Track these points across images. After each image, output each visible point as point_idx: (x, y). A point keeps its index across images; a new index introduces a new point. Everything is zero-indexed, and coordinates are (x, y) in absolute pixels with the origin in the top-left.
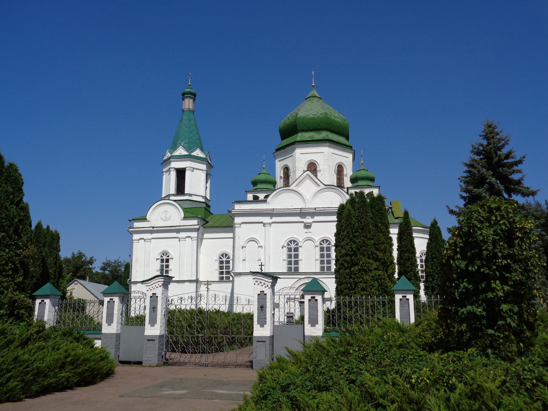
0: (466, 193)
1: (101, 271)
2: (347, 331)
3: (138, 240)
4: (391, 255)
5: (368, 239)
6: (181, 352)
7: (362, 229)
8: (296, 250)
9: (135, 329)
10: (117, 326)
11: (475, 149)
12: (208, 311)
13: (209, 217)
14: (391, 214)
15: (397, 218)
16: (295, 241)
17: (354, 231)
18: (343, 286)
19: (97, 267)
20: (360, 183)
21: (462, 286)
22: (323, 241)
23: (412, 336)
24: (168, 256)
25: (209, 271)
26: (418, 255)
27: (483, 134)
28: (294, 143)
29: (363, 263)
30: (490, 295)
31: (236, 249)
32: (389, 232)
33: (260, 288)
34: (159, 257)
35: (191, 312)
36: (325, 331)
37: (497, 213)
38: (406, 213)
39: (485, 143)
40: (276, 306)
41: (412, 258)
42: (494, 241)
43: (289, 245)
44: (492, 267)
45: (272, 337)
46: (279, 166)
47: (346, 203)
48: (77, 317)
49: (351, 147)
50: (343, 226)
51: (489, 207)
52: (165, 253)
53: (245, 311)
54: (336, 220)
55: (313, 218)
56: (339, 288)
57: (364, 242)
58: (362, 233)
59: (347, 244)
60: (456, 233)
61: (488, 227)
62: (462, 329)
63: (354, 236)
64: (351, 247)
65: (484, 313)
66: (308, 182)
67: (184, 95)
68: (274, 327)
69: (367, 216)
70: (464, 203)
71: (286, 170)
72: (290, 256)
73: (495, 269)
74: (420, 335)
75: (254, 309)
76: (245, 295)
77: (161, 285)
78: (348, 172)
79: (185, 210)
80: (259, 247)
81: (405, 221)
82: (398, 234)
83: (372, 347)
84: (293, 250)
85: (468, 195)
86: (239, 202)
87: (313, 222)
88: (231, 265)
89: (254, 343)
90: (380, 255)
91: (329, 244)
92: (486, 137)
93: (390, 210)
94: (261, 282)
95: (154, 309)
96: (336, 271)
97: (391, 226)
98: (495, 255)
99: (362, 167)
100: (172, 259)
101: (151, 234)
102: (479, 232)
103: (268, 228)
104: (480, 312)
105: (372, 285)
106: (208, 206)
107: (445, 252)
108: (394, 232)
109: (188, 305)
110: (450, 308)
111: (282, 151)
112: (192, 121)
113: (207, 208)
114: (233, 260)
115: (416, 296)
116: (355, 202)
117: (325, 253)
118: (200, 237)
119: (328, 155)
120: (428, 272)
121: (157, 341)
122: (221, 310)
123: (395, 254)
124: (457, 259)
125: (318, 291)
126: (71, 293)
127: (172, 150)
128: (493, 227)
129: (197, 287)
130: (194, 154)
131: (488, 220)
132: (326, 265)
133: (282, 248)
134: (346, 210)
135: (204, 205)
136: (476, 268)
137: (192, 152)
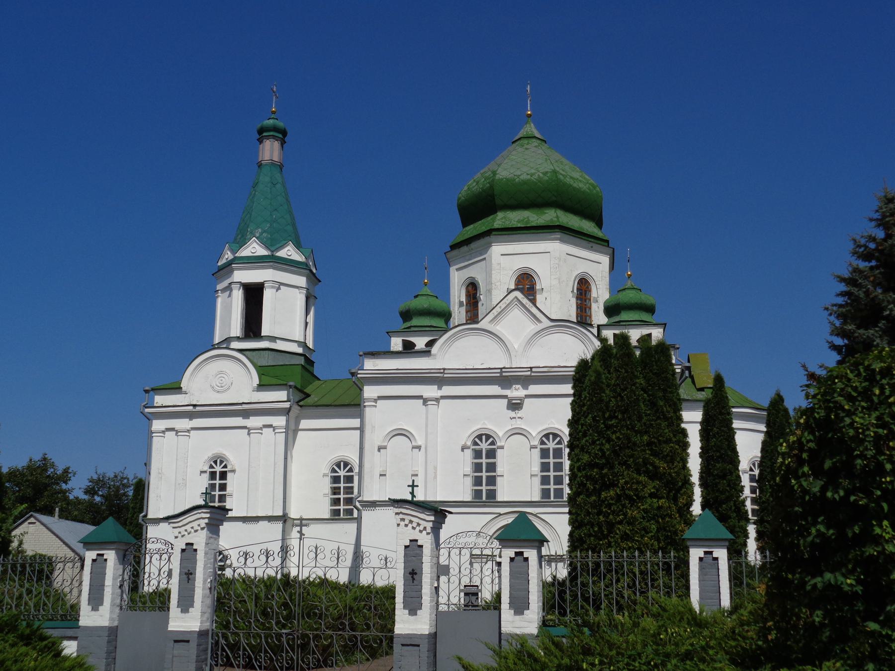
0: (843, 338)
1: (86, 497)
2: (586, 624)
3: (163, 432)
4: (685, 467)
5: (637, 432)
6: (245, 667)
7: (623, 413)
8: (491, 454)
9: (148, 617)
10: (111, 612)
11: (860, 246)
12: (304, 581)
13: (310, 385)
14: (689, 380)
15: (702, 389)
16: (488, 437)
17: (607, 415)
18: (584, 531)
19: (77, 488)
20: (625, 316)
21: (813, 531)
22: (547, 436)
23: (717, 635)
24: (225, 466)
25: (310, 497)
26: (744, 465)
27: (877, 216)
28: (488, 233)
29: (626, 483)
30: (871, 551)
31: (418, 450)
32: (680, 419)
33: (409, 534)
34: (206, 468)
35: (269, 583)
36: (544, 624)
37: (884, 381)
38: (719, 380)
39: (880, 234)
40: (442, 570)
41: (731, 473)
42: (877, 437)
43: (475, 444)
44: (873, 493)
45: (433, 637)
46: (457, 279)
47: (593, 358)
48: (29, 592)
49: (607, 241)
50: (584, 405)
51: (867, 368)
52: (218, 460)
53: (380, 583)
54: (572, 392)
55: (525, 387)
56: (576, 534)
57: (629, 439)
58: (624, 420)
59: (594, 442)
60: (802, 421)
61: (868, 409)
62: (814, 621)
63: (608, 427)
64: (601, 450)
65: (859, 589)
66: (516, 314)
67: (262, 133)
68: (440, 617)
69: (634, 384)
70: (839, 358)
71: (472, 288)
72: (478, 468)
73: (879, 497)
74: (734, 632)
75: (396, 577)
76: (381, 547)
77: (203, 525)
78: (601, 294)
79: (262, 371)
80: (414, 447)
81: (715, 395)
82: (702, 423)
83: (629, 657)
84: (484, 454)
85: (846, 341)
86: (373, 354)
87: (527, 396)
88: (356, 484)
89: (397, 647)
90: (662, 465)
91: (559, 443)
92: (882, 223)
93: (687, 372)
94: (411, 522)
95: (188, 575)
96: (572, 500)
97: (684, 405)
98: (880, 466)
99: (629, 284)
100: (233, 471)
101: (191, 419)
102: (848, 420)
103: (432, 408)
104: (851, 585)
105: (644, 529)
106: (310, 362)
107: (780, 460)
108: (692, 420)
109: (259, 569)
110: (790, 576)
111: (464, 249)
112: (278, 186)
113: (308, 367)
114: (360, 474)
115: (736, 551)
116: (611, 355)
117: (551, 460)
118: (292, 426)
119: (560, 259)
120: (764, 502)
121: (193, 644)
122: (328, 576)
123: (694, 464)
124: (804, 475)
125: (524, 540)
126: (21, 543)
127: (235, 246)
128: (876, 409)
129: (284, 531)
130: (282, 253)
131: (866, 394)
132: (552, 487)
133: (463, 450)
134: (590, 372)
135: (302, 361)
136: (842, 493)
137: (279, 249)
